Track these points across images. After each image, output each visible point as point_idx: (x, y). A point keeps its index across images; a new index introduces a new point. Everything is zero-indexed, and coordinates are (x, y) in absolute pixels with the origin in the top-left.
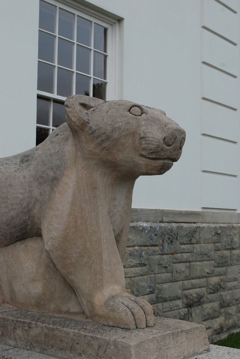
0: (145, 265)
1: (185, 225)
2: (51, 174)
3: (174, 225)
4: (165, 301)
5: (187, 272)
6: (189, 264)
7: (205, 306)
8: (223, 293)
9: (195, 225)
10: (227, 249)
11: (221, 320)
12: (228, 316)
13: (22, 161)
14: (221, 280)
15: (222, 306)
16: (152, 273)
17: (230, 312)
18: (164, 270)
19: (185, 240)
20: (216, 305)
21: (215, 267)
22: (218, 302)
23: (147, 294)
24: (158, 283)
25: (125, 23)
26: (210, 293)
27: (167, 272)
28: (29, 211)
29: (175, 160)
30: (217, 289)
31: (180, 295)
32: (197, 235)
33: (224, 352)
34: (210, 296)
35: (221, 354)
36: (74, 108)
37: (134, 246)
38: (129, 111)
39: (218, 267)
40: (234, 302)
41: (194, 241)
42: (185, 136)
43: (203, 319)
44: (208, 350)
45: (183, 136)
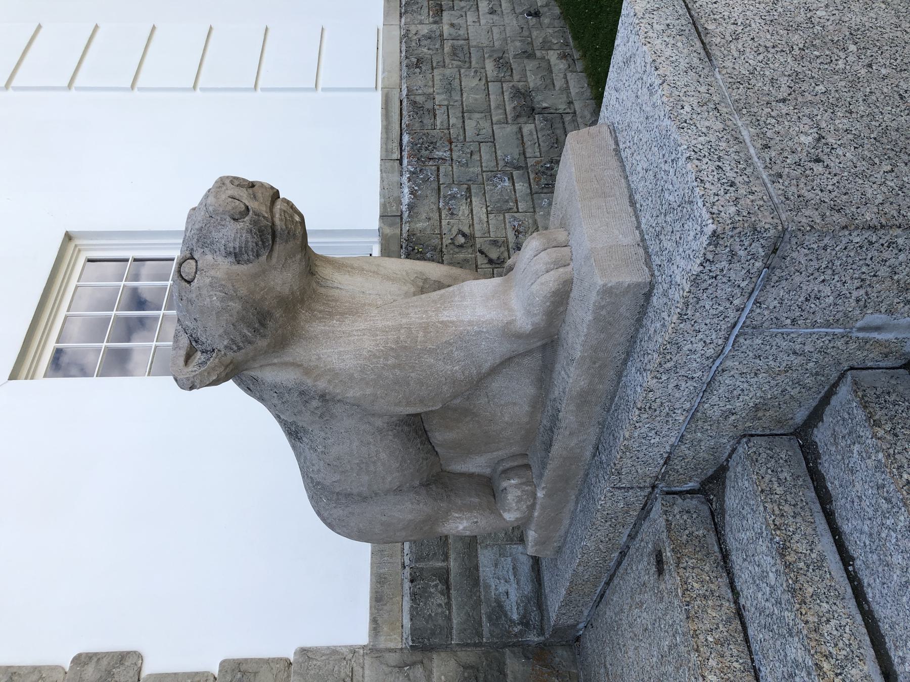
0: (469, 189)
1: (406, 120)
2: (315, 403)
3: (406, 138)
4: (524, 153)
5: (477, 116)
6: (467, 163)
7: (532, 85)
8: (511, 55)
9: (405, 103)
10: (442, 46)
11: (553, 56)
12: (546, 45)
13: (300, 439)
14: (490, 56)
15: (531, 56)
16: (480, 177)
17: (541, 40)
18: (476, 157)
19: (428, 121)
20: (530, 65)
21: (470, 67)
22: (526, 61)
23: (513, 185)
24: (497, 164)
25: (71, 229)
26: (511, 75)
27: (480, 151)
28: (380, 431)
29: (276, 195)
30: (502, 63)
31: (515, 128)
32: (420, 99)
33: (614, 98)
34: (516, 77)
35: (617, 106)
36: (194, 377)
37: (439, 209)
38: (189, 282)
39: (470, 62)
40: (526, 33)
41: (429, 105)
42: (228, 177)
43: (551, 87)
44: (613, 131)
45: (227, 182)
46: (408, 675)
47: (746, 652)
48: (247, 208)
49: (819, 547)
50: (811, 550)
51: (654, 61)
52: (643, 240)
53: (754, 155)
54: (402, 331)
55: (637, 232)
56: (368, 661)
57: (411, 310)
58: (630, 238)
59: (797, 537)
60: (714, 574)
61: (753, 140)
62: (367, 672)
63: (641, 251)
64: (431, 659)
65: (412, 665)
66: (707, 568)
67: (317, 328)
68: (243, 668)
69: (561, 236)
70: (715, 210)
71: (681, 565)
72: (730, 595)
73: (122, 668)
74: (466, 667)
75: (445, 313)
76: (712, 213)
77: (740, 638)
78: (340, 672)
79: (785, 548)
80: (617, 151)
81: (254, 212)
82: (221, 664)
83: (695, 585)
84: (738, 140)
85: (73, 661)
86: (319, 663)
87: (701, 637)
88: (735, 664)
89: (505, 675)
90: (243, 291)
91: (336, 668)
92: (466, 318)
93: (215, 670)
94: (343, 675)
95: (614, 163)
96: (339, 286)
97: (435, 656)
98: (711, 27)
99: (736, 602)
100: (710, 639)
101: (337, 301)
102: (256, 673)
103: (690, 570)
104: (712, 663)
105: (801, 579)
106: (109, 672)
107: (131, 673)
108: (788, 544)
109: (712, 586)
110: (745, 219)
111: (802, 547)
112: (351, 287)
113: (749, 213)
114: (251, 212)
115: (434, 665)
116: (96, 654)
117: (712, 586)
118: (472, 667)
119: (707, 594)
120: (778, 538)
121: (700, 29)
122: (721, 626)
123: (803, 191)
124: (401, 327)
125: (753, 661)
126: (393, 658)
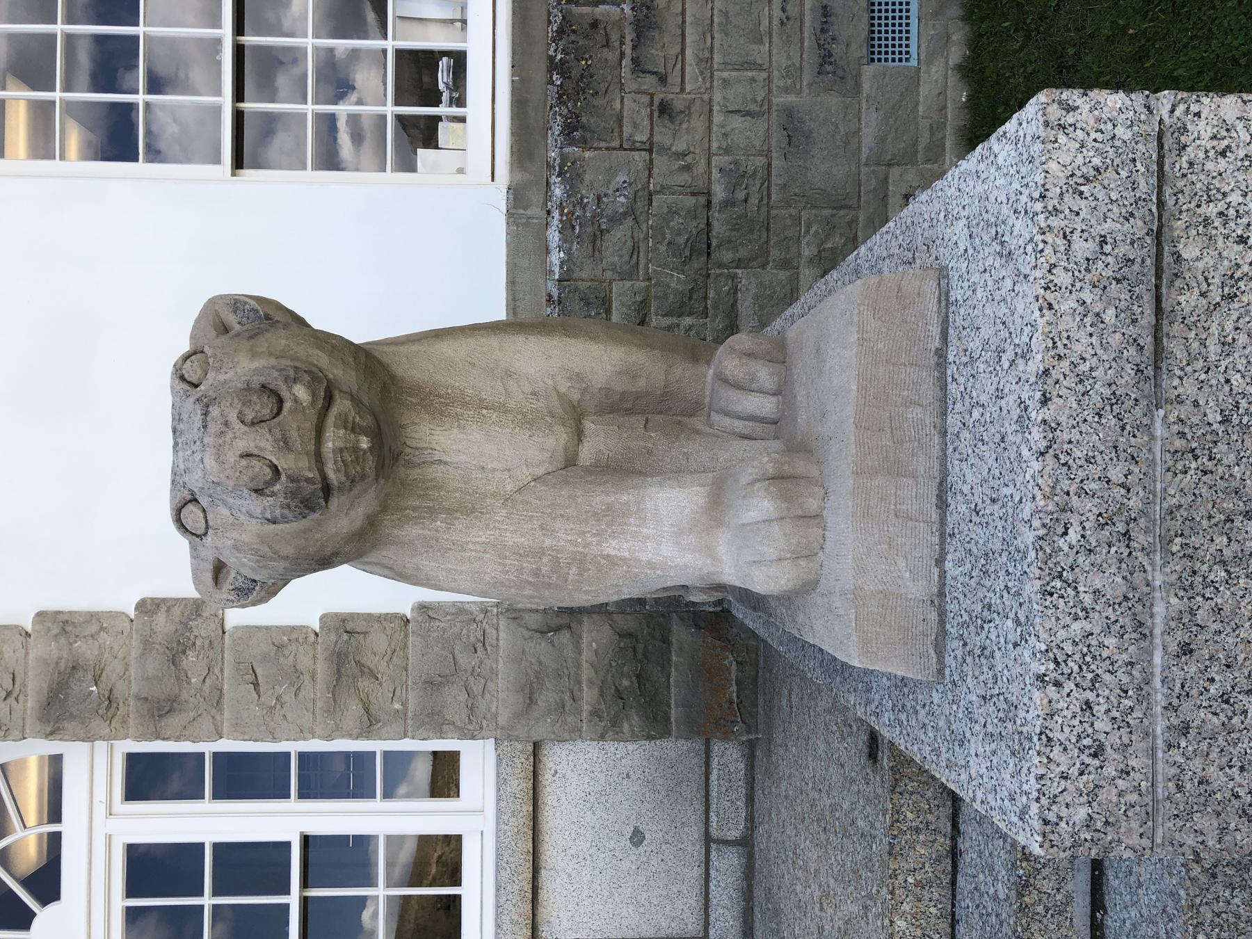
46: (552, 642)
47: (949, 896)
48: (276, 470)
49: (1069, 887)
50: (1058, 890)
51: (1046, 372)
52: (941, 594)
53: (1158, 670)
54: (545, 560)
55: (936, 571)
56: (503, 623)
57: (559, 524)
58: (918, 588)
59: (1046, 872)
60: (936, 802)
61: (1169, 631)
62: (502, 635)
63: (933, 616)
64: (580, 622)
65: (557, 629)
66: (929, 794)
67: (413, 531)
68: (349, 626)
69: (812, 504)
70: (1052, 817)
71: (898, 790)
72: (949, 829)
73: (200, 620)
74: (622, 635)
75: (614, 543)
76: (1046, 822)
77: (946, 880)
78: (469, 636)
79: (1027, 885)
80: (941, 354)
81: (288, 477)
82: (321, 619)
83: (910, 815)
84: (1142, 631)
85: (136, 609)
86: (442, 625)
87: (900, 877)
88: (933, 910)
89: (669, 644)
90: (289, 550)
91: (464, 632)
92: (644, 557)
93: (316, 626)
94: (472, 639)
95: (927, 381)
96: (445, 458)
97: (585, 619)
98: (1189, 251)
99: (953, 839)
100: (910, 880)
101: (440, 488)
102: (365, 633)
103: (907, 796)
104: (906, 907)
105: (1035, 927)
106: (186, 625)
107: (213, 626)
108: (1032, 881)
109: (930, 817)
110: (1096, 835)
111: (1047, 886)
112: (463, 458)
113: (1107, 823)
114: (283, 478)
115: (585, 628)
116: (164, 600)
117: (930, 817)
118: (630, 635)
119: (921, 826)
120: (1021, 872)
121: (1167, 258)
122: (927, 865)
123: (1212, 771)
124: (540, 553)
125: (953, 905)
126: (533, 620)
